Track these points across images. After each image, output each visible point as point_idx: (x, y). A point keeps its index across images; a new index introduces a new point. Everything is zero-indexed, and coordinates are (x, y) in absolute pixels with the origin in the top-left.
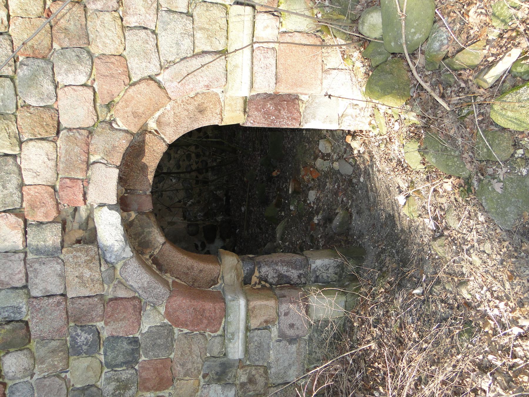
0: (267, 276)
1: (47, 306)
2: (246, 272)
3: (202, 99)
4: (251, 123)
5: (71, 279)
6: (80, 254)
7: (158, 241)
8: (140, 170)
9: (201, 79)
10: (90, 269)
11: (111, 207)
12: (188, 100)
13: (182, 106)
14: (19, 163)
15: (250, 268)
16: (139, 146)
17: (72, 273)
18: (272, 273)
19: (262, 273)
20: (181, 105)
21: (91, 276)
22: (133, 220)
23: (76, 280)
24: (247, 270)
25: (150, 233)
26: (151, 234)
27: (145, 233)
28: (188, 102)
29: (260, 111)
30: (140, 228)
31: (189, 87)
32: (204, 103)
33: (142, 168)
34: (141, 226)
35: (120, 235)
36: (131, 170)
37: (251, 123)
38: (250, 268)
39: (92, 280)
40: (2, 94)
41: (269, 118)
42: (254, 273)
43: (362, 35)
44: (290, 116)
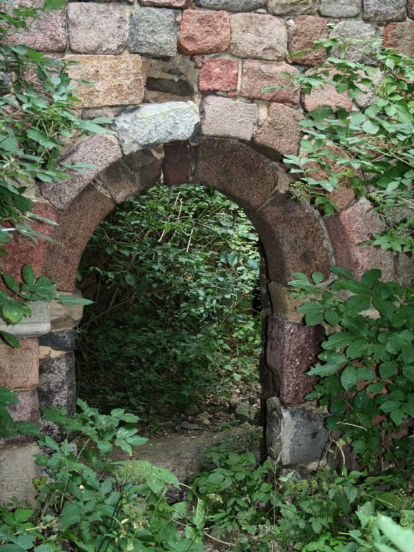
0: (51, 372)
1: (53, 25)
2: (60, 335)
3: (321, 257)
4: (290, 329)
5: (95, 63)
6: (131, 80)
7: (119, 192)
8: (225, 168)
9: (366, 253)
10: (109, 91)
11: (198, 128)
12: (319, 237)
13: (311, 229)
14: (259, 10)
15: (66, 342)
16: (258, 167)
17: (103, 64)
18: (57, 380)
19: (56, 363)
20: (312, 227)
21: (98, 91)
22: (152, 155)
23: (92, 70)
24: (64, 337)
25: (133, 180)
26: (131, 181)
27: (133, 173)
28: (317, 238)
29: (306, 343)
30: (141, 165)
31: (356, 238)
32: (316, 260)
33: (227, 171)
34: (143, 167)
35: (158, 137)
36: (225, 156)
37: (290, 329)
38: (66, 342)
39: (91, 93)
40: (342, 2)
41: (297, 357)
42: (56, 350)
43: (63, 506)
44: (300, 388)
